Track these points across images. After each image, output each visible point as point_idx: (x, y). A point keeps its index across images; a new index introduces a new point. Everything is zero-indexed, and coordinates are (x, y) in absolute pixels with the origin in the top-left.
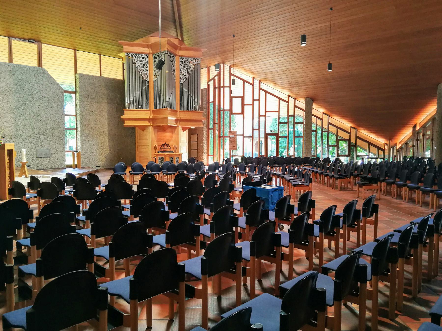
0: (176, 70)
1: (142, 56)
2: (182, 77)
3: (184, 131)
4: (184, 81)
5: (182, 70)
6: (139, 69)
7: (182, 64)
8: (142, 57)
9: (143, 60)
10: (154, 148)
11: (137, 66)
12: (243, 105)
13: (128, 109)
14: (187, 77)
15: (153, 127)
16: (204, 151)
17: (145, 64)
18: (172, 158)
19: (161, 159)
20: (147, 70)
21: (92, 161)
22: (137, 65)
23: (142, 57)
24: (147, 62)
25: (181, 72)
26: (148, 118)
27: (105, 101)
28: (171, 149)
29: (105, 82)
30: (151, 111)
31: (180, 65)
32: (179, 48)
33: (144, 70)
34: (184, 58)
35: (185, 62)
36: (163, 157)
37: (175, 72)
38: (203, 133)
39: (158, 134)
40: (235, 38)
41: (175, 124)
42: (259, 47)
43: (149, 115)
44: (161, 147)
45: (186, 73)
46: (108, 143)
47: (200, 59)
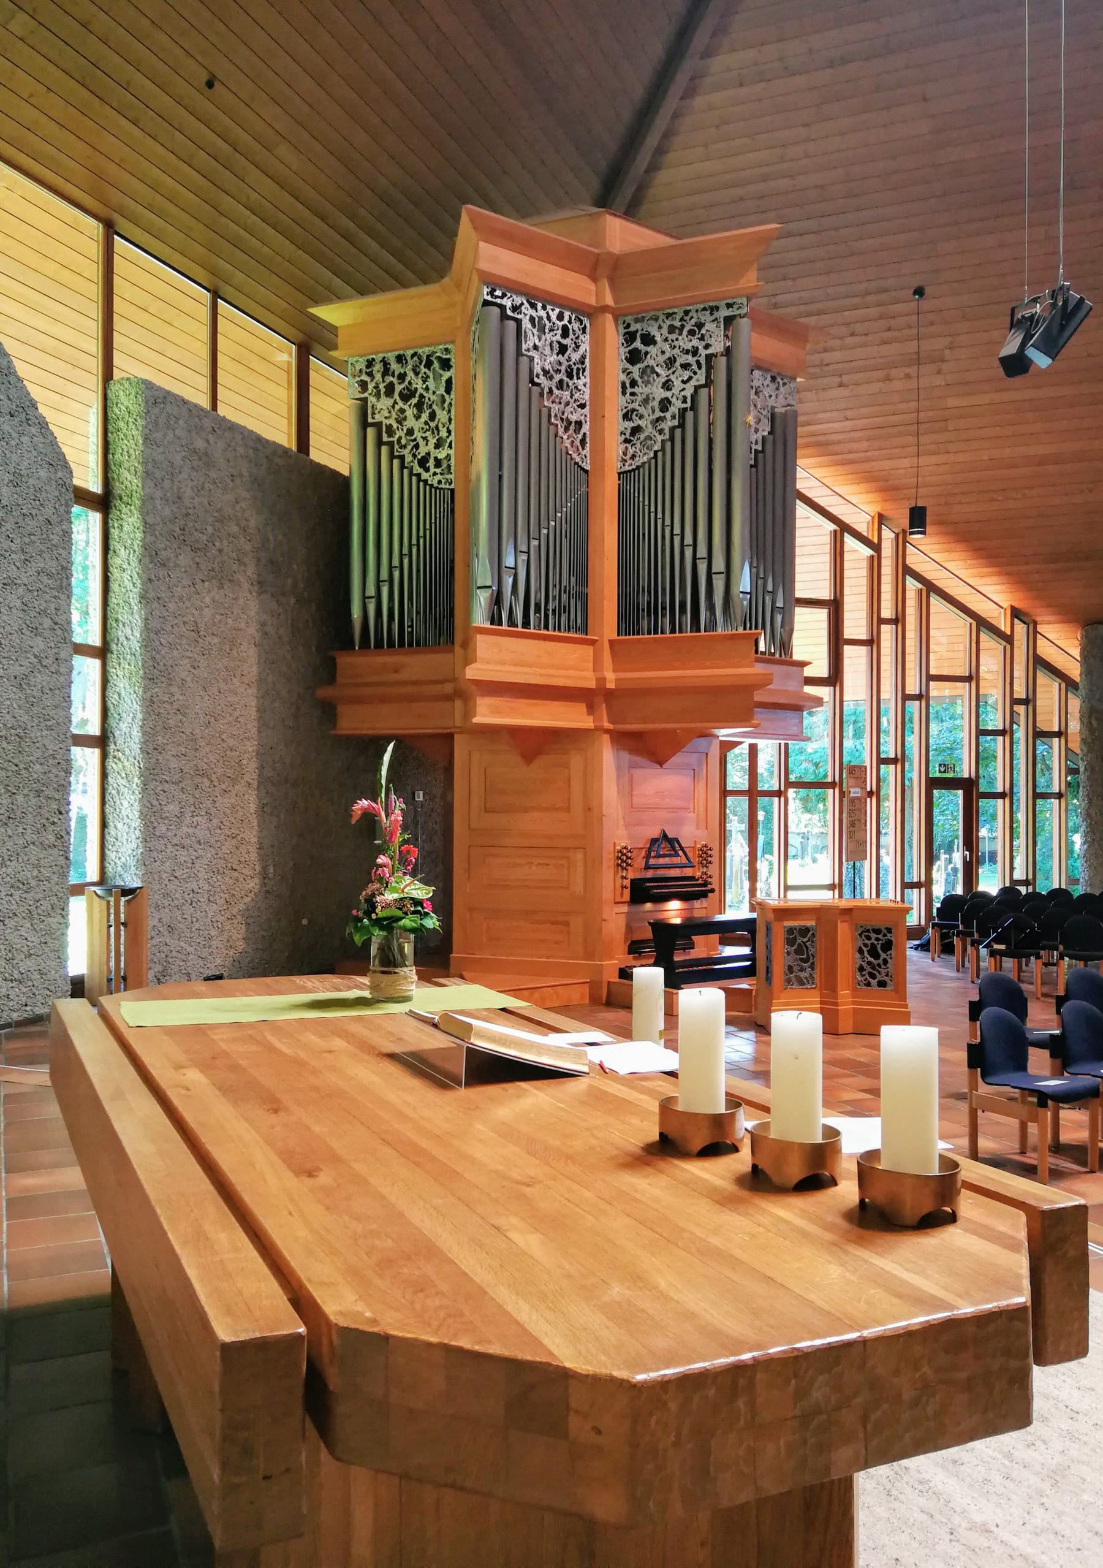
1: (560, 317)
8: (560, 324)
12: (837, 641)
13: (505, 627)
17: (575, 368)
20: (582, 406)
21: (189, 949)
23: (560, 324)
24: (584, 357)
30: (606, 645)
36: (811, 923)
40: (926, 304)
44: (648, 857)
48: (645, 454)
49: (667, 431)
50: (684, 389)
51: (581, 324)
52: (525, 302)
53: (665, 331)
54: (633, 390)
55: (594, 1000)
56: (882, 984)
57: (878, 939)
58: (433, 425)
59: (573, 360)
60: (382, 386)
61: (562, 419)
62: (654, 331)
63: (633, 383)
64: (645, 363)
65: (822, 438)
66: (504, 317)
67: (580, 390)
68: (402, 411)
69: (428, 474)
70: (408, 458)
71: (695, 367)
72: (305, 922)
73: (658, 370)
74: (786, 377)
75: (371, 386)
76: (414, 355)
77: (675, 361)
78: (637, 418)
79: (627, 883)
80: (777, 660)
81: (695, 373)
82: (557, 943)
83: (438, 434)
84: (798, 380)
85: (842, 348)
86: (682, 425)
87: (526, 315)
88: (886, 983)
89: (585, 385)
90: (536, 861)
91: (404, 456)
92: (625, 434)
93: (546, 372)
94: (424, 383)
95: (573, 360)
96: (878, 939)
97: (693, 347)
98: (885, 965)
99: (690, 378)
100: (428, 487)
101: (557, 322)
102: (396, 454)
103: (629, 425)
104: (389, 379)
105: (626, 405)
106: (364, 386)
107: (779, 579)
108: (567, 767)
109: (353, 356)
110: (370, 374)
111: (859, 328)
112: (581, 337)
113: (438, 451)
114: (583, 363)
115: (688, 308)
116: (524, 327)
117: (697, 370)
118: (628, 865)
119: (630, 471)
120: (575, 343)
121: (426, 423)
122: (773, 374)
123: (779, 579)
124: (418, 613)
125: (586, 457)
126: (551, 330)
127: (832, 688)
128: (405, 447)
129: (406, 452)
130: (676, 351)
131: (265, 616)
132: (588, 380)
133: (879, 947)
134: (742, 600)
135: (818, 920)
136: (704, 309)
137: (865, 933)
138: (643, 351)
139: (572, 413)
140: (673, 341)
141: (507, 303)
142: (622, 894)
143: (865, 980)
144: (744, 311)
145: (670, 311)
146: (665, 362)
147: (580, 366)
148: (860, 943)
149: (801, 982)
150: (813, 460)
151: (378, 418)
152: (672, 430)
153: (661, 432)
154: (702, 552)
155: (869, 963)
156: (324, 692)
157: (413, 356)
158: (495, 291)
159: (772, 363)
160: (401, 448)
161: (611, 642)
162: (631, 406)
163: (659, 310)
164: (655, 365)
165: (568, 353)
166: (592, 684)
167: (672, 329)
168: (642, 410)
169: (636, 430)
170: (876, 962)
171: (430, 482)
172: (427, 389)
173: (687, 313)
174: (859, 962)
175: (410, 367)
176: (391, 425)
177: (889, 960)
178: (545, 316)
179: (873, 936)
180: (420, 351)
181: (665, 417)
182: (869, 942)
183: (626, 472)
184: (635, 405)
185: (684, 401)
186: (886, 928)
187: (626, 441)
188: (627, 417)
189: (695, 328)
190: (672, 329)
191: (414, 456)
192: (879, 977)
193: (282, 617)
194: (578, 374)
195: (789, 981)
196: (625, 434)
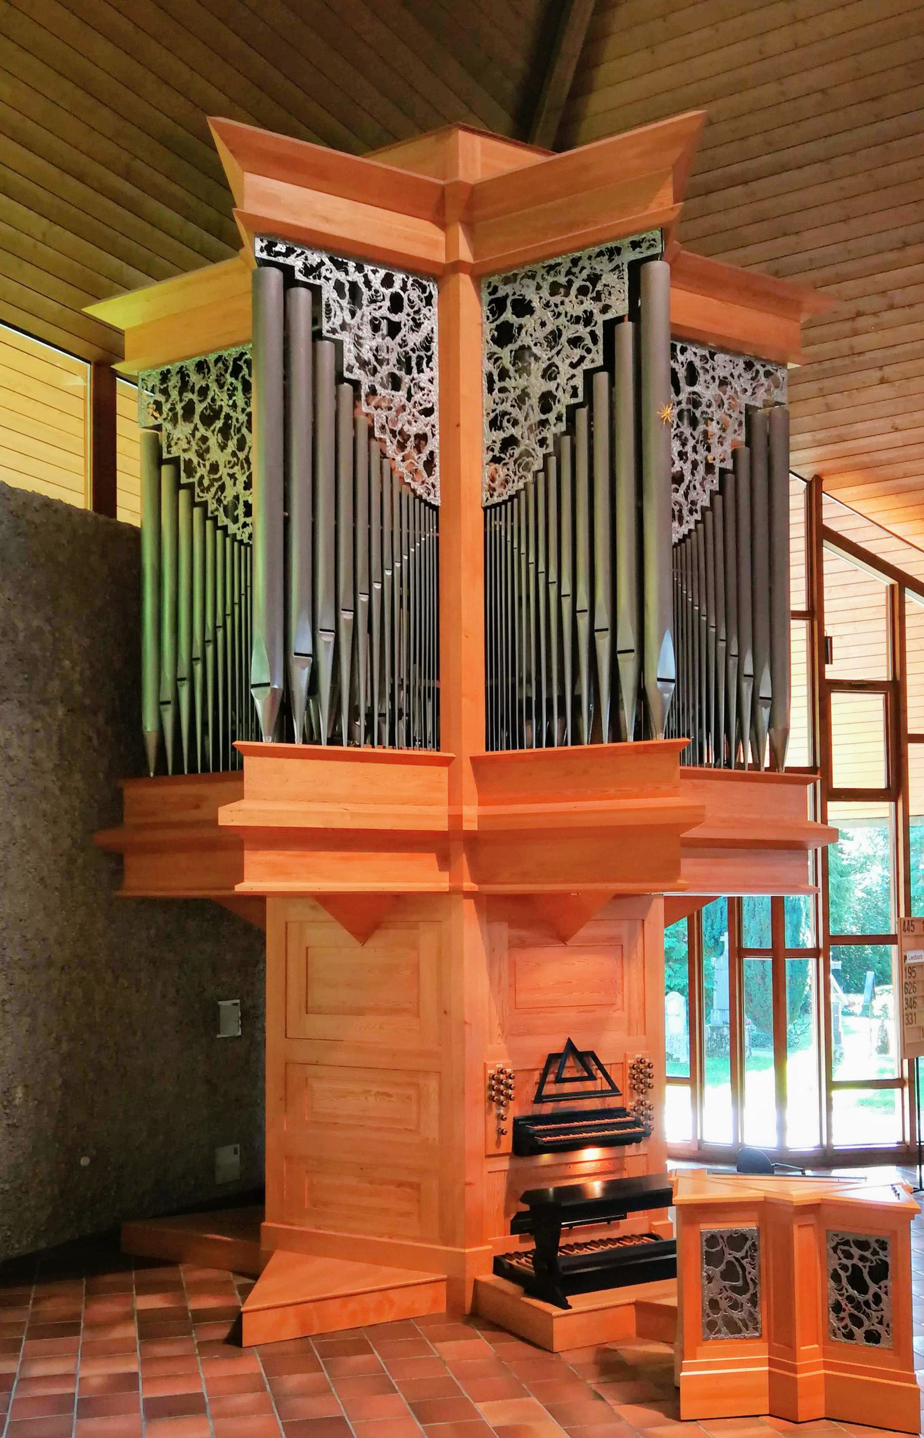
1: (388, 281)
4: (684, 530)
6: (364, 390)
8: (388, 292)
13: (298, 744)
14: (707, 503)
15: (477, 903)
17: (414, 356)
20: (428, 412)
22: (349, 358)
23: (388, 292)
24: (429, 340)
28: (614, 1091)
30: (467, 766)
35: (692, 379)
36: (748, 1226)
42: (829, 408)
44: (542, 1083)
47: (780, 374)
48: (520, 478)
49: (550, 441)
50: (573, 376)
51: (424, 292)
52: (326, 260)
53: (545, 292)
54: (502, 384)
55: (454, 1310)
56: (873, 1337)
57: (862, 1258)
58: (242, 455)
59: (411, 345)
60: (179, 408)
61: (393, 432)
62: (530, 294)
63: (504, 374)
64: (519, 343)
65: (865, 458)
66: (289, 281)
67: (422, 389)
68: (204, 439)
69: (236, 526)
70: (212, 506)
71: (588, 341)
72: (85, 1161)
73: (535, 350)
74: (769, 361)
75: (166, 408)
76: (219, 359)
77: (560, 335)
78: (509, 425)
79: (508, 1126)
81: (589, 351)
82: (403, 1214)
83: (249, 468)
84: (790, 366)
85: (879, 328)
86: (571, 429)
87: (327, 279)
88: (879, 1335)
89: (431, 381)
90: (375, 1089)
91: (206, 502)
92: (493, 450)
93: (363, 364)
94: (230, 398)
95: (411, 345)
96: (862, 1258)
97: (585, 312)
98: (877, 1304)
99: (582, 359)
100: (236, 544)
101: (383, 290)
102: (197, 500)
103: (499, 435)
104: (188, 396)
105: (495, 406)
106: (158, 406)
107: (764, 655)
108: (414, 946)
109: (145, 369)
110: (165, 392)
111: (898, 297)
112: (425, 311)
113: (248, 492)
114: (428, 349)
115: (578, 254)
116: (325, 296)
117: (591, 345)
118: (509, 1097)
119: (499, 504)
120: (414, 319)
121: (234, 454)
122: (747, 359)
123: (764, 655)
124: (241, 721)
125: (434, 486)
126: (372, 301)
127: (893, 803)
128: (208, 489)
129: (208, 497)
130: (562, 320)
131: (8, 734)
132: (436, 373)
134: (661, 693)
135: (762, 1221)
136: (600, 254)
137: (842, 1245)
138: (516, 325)
139: (409, 423)
140: (556, 306)
141: (297, 263)
142: (498, 1143)
143: (845, 1327)
144: (658, 250)
145: (552, 262)
146: (546, 337)
147: (422, 353)
149: (734, 1328)
150: (854, 490)
151: (175, 452)
152: (557, 439)
153: (542, 442)
154: (603, 619)
155: (850, 1299)
156: (107, 837)
157: (217, 361)
158: (275, 245)
159: (744, 343)
160: (202, 491)
162: (500, 408)
163: (536, 261)
164: (532, 344)
165: (401, 334)
166: (442, 825)
167: (555, 289)
168: (516, 413)
169: (510, 442)
170: (861, 1298)
171: (239, 538)
172: (234, 406)
173: (575, 262)
174: (834, 1296)
175: (213, 377)
176: (190, 461)
177: (883, 1296)
178: (360, 280)
179: (856, 1252)
180: (225, 354)
181: (547, 420)
182: (849, 1263)
183: (494, 506)
184: (506, 407)
185: (574, 394)
186: (877, 1241)
187: (496, 460)
188: (494, 424)
189: (588, 284)
190: (555, 289)
191: (219, 501)
192: (867, 1325)
193: (42, 734)
194: (419, 365)
195: (711, 1326)
196: (493, 450)
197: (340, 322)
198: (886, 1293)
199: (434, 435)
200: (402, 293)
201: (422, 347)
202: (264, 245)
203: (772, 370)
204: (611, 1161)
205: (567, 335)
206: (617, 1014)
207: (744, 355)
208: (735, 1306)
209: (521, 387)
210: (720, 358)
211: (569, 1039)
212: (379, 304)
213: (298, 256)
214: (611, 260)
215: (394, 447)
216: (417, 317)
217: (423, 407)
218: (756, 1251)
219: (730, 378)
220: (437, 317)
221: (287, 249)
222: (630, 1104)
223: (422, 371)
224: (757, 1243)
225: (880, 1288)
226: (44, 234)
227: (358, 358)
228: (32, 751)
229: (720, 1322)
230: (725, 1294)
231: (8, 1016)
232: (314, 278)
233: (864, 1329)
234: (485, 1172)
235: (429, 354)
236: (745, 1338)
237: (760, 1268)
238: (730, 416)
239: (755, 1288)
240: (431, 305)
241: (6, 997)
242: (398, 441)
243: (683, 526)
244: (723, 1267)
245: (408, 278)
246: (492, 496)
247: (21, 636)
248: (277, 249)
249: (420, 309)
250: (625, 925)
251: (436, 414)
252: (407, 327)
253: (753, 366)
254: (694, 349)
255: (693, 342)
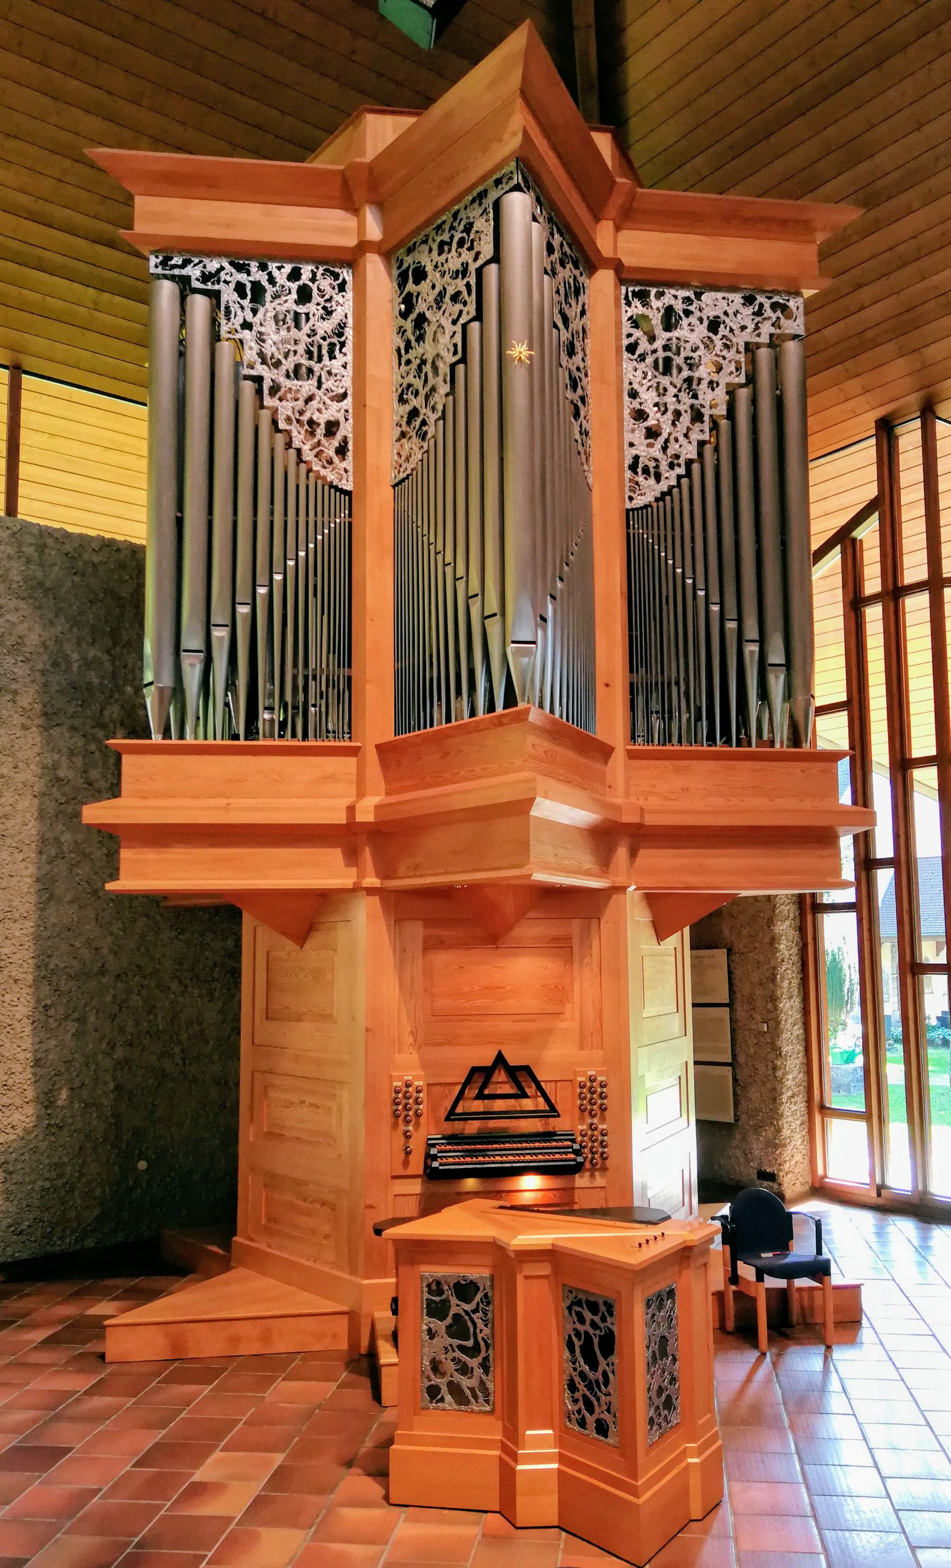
0: (590, 386)
1: (295, 275)
2: (647, 452)
3: (661, 934)
4: (663, 486)
5: (641, 391)
7: (644, 346)
8: (294, 286)
9: (302, 309)
10: (387, 1110)
11: (251, 367)
13: (157, 738)
16: (790, 1080)
18: (593, 1307)
19: (457, 1306)
22: (250, 355)
24: (342, 326)
25: (640, 415)
26: (341, 818)
27: (25, 700)
28: (552, 1111)
29: (28, 561)
30: (372, 755)
31: (632, 348)
32: (617, 201)
33: (310, 399)
34: (660, 295)
35: (668, 325)
36: (478, 1273)
37: (583, 399)
38: (773, 941)
39: (428, 973)
41: (595, 868)
43: (353, 790)
45: (678, 414)
46: (27, 1043)
52: (226, 265)
57: (594, 1325)
59: (321, 333)
63: (408, 346)
72: (142, 1165)
74: (776, 292)
80: (808, 753)
81: (465, 304)
89: (344, 367)
92: (401, 426)
95: (321, 333)
96: (594, 1325)
114: (340, 335)
120: (324, 308)
125: (346, 471)
132: (349, 358)
133: (596, 1341)
139: (319, 410)
141: (194, 272)
142: (406, 1163)
143: (579, 1412)
147: (335, 340)
148: (569, 1327)
158: (171, 258)
161: (381, 749)
170: (591, 1375)
173: (455, 216)
179: (588, 1315)
197: (241, 321)
198: (613, 1372)
199: (347, 420)
200: (310, 284)
201: (334, 333)
202: (158, 261)
203: (781, 301)
204: (554, 1192)
205: (451, 291)
206: (563, 1025)
207: (742, 290)
208: (465, 1370)
209: (420, 356)
210: (707, 297)
211: (500, 1053)
212: (284, 298)
213: (195, 265)
214: (480, 204)
215: (302, 437)
216: (328, 305)
217: (334, 393)
218: (488, 1304)
219: (723, 317)
220: (351, 303)
221: (184, 260)
222: (580, 1127)
223: (335, 358)
224: (489, 1295)
225: (608, 1364)
226: (95, 303)
227: (261, 355)
228: (85, 772)
229: (444, 1389)
230: (451, 1355)
231: (51, 1021)
232: (213, 283)
233: (595, 1416)
234: (390, 1198)
235: (343, 339)
236: (472, 1411)
237: (493, 1324)
238: (724, 358)
239: (487, 1350)
240: (345, 291)
241: (49, 1002)
242: (306, 431)
243: (662, 483)
244: (449, 1320)
245: (317, 268)
246: (399, 472)
247: (75, 666)
248: (173, 262)
249: (331, 297)
250: (576, 925)
251: (349, 399)
252: (316, 317)
253: (756, 299)
254: (673, 292)
255: (670, 285)
